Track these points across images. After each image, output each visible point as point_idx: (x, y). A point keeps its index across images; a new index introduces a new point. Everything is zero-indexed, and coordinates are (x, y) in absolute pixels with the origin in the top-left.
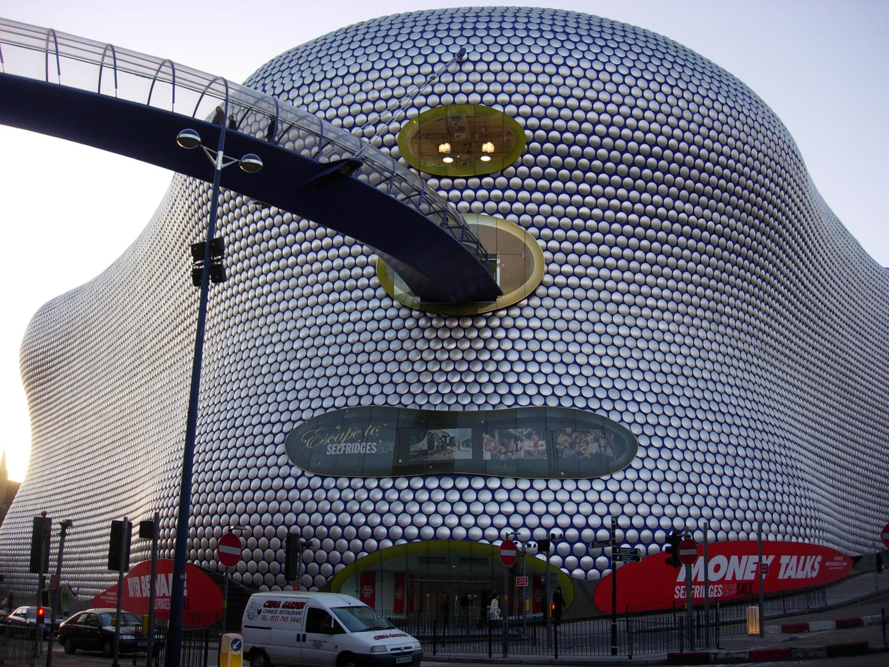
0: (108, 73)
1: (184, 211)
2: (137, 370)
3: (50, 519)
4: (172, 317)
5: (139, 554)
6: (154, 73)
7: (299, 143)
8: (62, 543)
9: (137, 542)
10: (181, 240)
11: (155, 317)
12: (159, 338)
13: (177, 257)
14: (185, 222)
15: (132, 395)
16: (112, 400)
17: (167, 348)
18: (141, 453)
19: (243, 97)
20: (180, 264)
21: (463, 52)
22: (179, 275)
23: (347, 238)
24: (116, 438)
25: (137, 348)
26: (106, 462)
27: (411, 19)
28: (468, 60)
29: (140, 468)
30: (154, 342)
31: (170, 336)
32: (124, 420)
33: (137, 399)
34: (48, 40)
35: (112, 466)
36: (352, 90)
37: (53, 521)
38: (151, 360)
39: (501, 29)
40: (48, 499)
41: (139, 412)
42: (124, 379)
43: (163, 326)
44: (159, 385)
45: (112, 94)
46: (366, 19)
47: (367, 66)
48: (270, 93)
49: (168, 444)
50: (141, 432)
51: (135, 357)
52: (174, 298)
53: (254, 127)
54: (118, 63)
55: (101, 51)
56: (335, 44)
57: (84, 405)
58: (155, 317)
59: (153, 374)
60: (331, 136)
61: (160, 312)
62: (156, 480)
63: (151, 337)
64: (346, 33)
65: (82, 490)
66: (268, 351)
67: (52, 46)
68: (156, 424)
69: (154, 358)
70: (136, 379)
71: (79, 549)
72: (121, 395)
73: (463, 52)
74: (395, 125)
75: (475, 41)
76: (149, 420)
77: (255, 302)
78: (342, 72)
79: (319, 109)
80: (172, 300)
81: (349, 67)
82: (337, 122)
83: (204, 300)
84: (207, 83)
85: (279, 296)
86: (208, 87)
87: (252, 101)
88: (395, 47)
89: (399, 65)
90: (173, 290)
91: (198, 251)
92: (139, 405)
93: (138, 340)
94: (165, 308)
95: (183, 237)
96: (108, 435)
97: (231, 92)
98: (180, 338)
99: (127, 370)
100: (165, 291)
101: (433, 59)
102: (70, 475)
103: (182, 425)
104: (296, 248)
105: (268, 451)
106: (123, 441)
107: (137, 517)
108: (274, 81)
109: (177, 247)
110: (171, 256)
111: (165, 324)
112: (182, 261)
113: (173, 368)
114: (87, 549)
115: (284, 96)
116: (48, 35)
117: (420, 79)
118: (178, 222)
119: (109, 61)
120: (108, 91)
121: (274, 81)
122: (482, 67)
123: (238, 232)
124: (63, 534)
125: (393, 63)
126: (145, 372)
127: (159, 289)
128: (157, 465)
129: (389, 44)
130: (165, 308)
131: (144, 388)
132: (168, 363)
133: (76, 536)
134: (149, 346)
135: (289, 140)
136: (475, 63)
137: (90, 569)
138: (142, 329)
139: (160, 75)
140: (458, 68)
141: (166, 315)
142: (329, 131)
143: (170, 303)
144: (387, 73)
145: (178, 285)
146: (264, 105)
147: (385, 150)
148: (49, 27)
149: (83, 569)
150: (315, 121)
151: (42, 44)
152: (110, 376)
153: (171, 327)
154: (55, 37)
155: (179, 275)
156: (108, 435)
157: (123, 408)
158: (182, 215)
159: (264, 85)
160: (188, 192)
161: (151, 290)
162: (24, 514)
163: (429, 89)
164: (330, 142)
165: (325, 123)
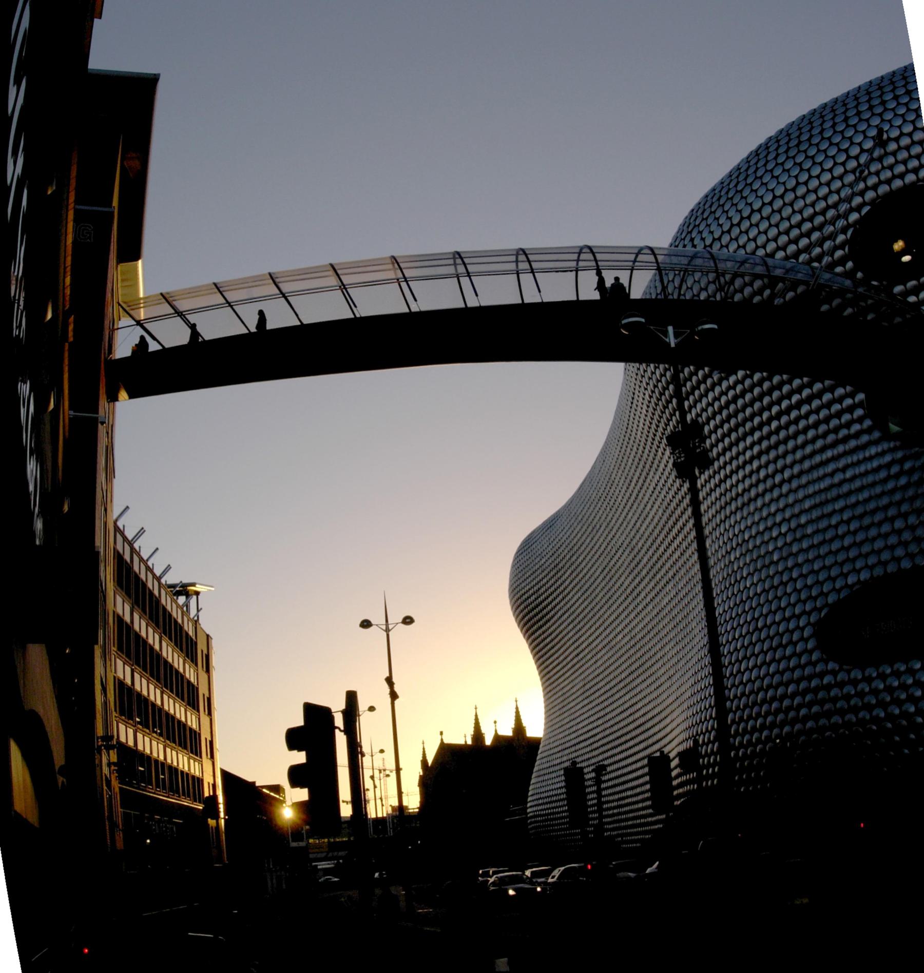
0: (527, 279)
1: (646, 402)
2: (639, 589)
3: (582, 768)
4: (662, 522)
5: (681, 790)
6: (574, 264)
7: (748, 291)
8: (599, 791)
9: (677, 777)
10: (651, 435)
11: (644, 526)
12: (654, 547)
13: (652, 455)
14: (650, 414)
15: (640, 617)
16: (620, 628)
17: (665, 557)
18: (663, 679)
19: (675, 260)
20: (656, 462)
21: (880, 131)
22: (659, 473)
23: (827, 383)
24: (633, 668)
25: (633, 565)
26: (627, 697)
27: (817, 116)
28: (889, 139)
29: (664, 696)
30: (650, 553)
31: (666, 543)
32: (638, 646)
33: (646, 621)
34: (455, 264)
35: (634, 700)
36: (784, 214)
37: (586, 770)
38: (651, 574)
39: (896, 98)
40: (573, 749)
41: (652, 634)
42: (627, 602)
43: (655, 534)
44: (666, 600)
45: (476, 304)
46: (772, 133)
47: (792, 183)
48: (700, 248)
49: (690, 664)
50: (658, 656)
51: (633, 574)
52: (660, 500)
53: (699, 288)
54: (534, 265)
55: (513, 258)
56: (750, 171)
57: (591, 639)
58: (644, 526)
59: (657, 589)
60: (778, 272)
61: (648, 520)
62: (685, 706)
63: (645, 549)
64: (758, 155)
65: (607, 732)
66: (775, 534)
67: (461, 269)
68: (672, 644)
69: (654, 571)
70: (640, 598)
71: (616, 797)
72: (627, 621)
73: (880, 131)
74: (841, 238)
75: (888, 116)
76: (664, 641)
77: (747, 482)
78: (768, 199)
79: (757, 247)
80: (658, 503)
81: (773, 190)
82: (780, 255)
83: (694, 491)
84: (632, 257)
85: (771, 468)
86: (635, 261)
87: (685, 261)
88: (812, 152)
89: (823, 170)
90: (656, 492)
91: (674, 441)
92: (650, 626)
93: (632, 555)
94: (652, 513)
95: (652, 430)
96: (624, 667)
97: (660, 258)
98: (677, 542)
99: (628, 591)
100: (648, 495)
101: (855, 151)
102: (592, 719)
103: (700, 637)
104: (775, 409)
105: (799, 648)
106: (641, 670)
107: (674, 750)
108: (700, 232)
109: (649, 443)
110: (645, 455)
111: (657, 531)
112: (658, 458)
113: (677, 578)
114: (624, 795)
115: (717, 246)
116: (454, 258)
117: (850, 178)
118: (643, 416)
119: (524, 266)
120: (531, 297)
121: (700, 232)
122: (905, 141)
123: (710, 410)
124: (598, 781)
125: (816, 171)
126: (648, 589)
127: (641, 495)
128: (683, 689)
129: (805, 151)
130: (652, 513)
131: (650, 607)
132: (671, 573)
133: (610, 784)
134: (645, 559)
135: (736, 291)
136: (897, 140)
137: (631, 815)
138: (634, 542)
139: (581, 264)
140: (882, 151)
141: (656, 520)
142: (775, 267)
143: (656, 506)
144: (814, 184)
145: (660, 484)
146: (698, 262)
147: (839, 269)
148: (453, 250)
149: (624, 817)
150: (758, 261)
151: (451, 270)
152: (611, 602)
153: (664, 532)
154: (462, 258)
155: (659, 473)
156: (624, 667)
157: (633, 633)
158: (645, 407)
159: (692, 240)
160: (645, 380)
161: (633, 498)
162: (551, 770)
163: (862, 185)
164: (782, 279)
165: (770, 261)
